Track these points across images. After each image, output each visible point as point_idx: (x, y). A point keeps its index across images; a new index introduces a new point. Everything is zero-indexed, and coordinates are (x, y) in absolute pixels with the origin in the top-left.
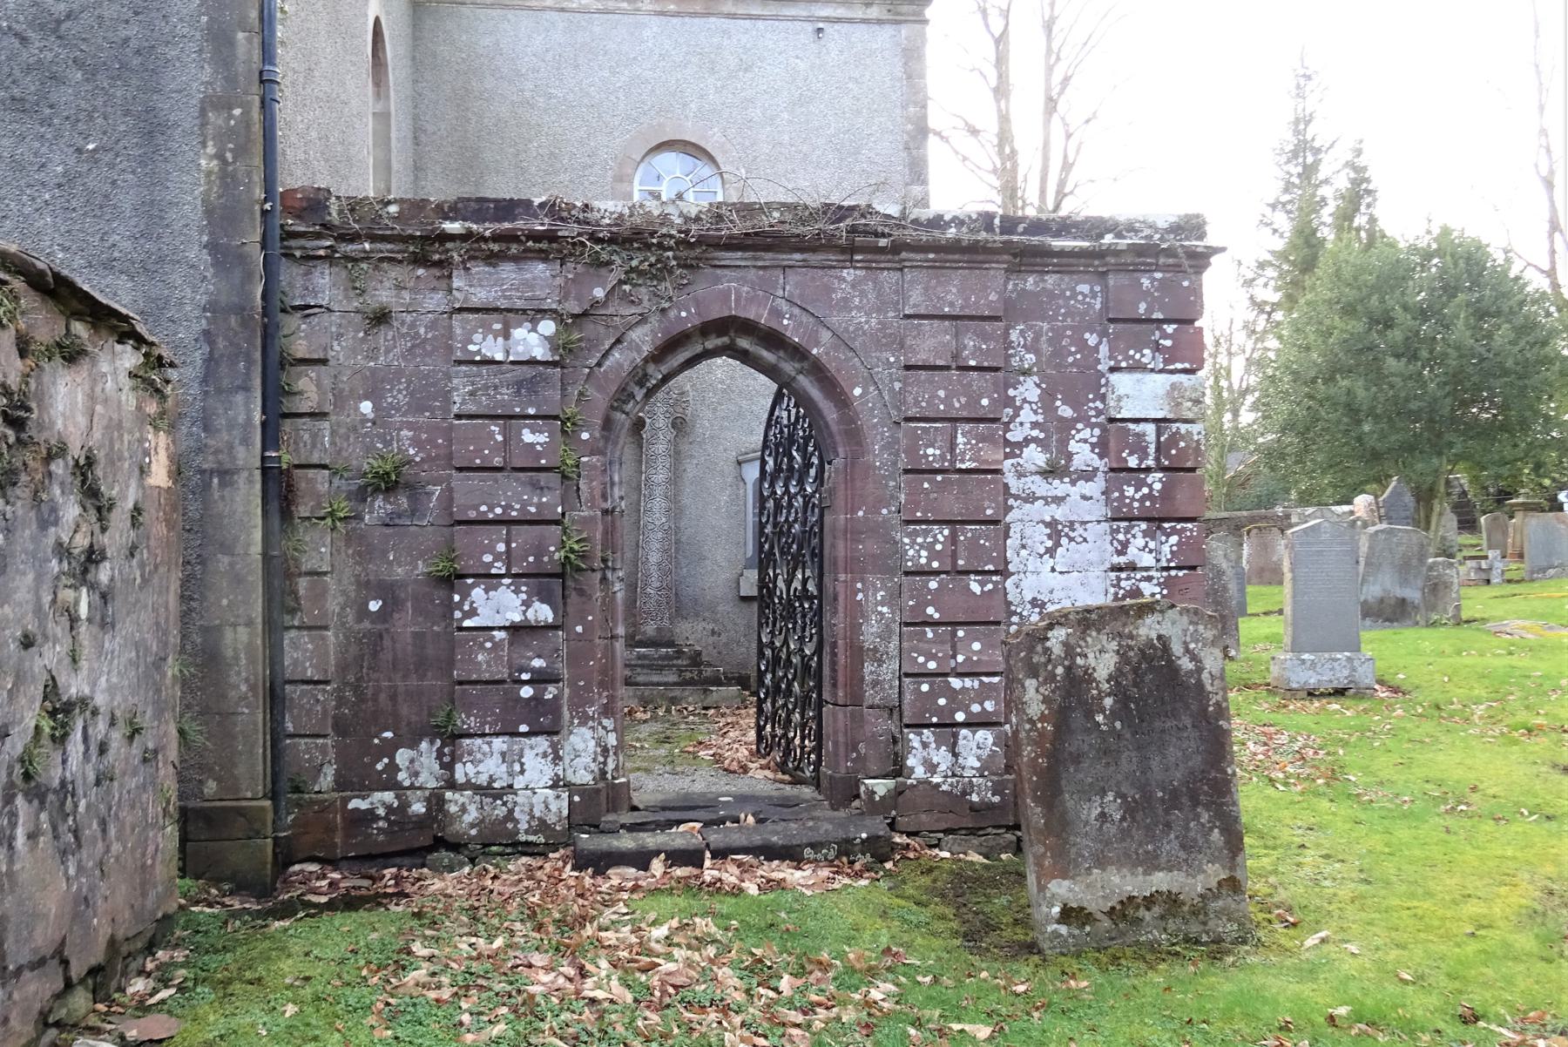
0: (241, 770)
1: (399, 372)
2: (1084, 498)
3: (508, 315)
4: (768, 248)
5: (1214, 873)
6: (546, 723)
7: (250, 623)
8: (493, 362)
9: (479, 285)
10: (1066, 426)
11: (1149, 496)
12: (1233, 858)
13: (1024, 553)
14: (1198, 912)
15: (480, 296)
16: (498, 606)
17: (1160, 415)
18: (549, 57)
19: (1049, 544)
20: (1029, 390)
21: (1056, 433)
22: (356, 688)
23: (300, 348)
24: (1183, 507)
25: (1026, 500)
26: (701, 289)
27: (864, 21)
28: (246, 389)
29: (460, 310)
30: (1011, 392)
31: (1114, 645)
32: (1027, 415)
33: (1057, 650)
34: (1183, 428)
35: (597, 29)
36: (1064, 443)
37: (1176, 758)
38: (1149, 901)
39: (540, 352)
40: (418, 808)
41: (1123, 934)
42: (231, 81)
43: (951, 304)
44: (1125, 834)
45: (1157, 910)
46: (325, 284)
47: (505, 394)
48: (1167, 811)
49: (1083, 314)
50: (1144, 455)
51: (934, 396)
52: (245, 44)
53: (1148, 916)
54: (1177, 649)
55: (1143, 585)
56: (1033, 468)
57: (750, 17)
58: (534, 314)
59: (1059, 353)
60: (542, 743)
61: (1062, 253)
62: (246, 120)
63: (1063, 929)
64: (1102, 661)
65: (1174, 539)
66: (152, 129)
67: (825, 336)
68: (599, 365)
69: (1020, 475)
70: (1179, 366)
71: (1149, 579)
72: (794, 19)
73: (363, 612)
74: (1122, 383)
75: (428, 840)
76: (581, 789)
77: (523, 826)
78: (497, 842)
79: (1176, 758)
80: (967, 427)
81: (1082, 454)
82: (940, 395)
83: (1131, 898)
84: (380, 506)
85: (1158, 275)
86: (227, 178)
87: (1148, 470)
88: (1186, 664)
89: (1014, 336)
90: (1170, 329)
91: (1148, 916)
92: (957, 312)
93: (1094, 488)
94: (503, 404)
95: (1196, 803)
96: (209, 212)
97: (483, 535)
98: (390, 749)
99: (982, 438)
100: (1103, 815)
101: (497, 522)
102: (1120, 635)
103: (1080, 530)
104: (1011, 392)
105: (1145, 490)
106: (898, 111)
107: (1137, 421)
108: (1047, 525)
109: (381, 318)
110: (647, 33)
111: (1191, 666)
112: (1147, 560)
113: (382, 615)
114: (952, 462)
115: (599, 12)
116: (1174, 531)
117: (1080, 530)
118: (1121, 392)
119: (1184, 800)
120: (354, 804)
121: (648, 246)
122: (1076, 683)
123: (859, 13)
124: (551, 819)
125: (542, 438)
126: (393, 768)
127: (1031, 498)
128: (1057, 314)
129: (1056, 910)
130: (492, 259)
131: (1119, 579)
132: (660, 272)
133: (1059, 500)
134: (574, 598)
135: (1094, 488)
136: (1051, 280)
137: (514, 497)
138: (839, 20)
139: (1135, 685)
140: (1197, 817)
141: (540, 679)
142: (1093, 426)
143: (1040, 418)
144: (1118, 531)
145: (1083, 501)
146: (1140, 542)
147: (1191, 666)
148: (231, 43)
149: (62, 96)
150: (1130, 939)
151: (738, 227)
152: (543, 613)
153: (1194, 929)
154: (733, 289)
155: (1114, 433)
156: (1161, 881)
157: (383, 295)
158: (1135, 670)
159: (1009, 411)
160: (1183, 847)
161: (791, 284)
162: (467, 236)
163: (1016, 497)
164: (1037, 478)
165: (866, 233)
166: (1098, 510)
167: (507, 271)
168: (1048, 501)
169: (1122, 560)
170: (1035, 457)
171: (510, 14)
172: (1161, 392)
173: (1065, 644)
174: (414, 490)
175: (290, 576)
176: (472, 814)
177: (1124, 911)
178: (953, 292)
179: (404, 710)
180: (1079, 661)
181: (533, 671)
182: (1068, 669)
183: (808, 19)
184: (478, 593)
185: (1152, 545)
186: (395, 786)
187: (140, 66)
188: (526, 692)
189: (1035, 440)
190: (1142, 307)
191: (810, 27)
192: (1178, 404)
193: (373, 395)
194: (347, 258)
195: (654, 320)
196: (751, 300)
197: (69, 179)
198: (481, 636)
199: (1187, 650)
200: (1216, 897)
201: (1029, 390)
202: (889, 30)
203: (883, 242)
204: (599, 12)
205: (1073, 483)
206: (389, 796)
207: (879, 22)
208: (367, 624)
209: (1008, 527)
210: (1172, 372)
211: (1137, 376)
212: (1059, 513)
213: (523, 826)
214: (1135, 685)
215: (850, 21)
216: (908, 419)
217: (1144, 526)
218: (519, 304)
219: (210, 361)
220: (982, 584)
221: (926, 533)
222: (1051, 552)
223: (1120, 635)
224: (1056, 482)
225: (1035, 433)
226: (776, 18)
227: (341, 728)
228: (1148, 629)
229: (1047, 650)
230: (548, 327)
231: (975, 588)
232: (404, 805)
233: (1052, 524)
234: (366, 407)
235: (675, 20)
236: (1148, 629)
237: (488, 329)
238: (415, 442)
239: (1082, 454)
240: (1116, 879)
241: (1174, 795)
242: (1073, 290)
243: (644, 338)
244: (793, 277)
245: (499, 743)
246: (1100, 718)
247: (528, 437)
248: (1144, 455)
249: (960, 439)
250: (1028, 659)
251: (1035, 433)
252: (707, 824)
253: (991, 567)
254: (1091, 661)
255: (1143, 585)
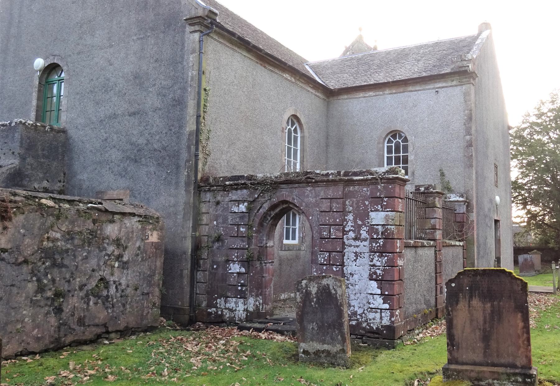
0: (185, 300)
1: (221, 215)
2: (364, 246)
3: (239, 202)
4: (290, 183)
5: (339, 347)
6: (243, 296)
7: (187, 269)
8: (235, 212)
9: (235, 195)
10: (360, 227)
11: (379, 246)
12: (344, 344)
13: (348, 260)
14: (334, 356)
15: (234, 198)
16: (235, 268)
17: (383, 223)
18: (361, 111)
19: (355, 258)
20: (350, 217)
21: (357, 229)
22: (211, 285)
23: (204, 210)
24: (389, 248)
25: (349, 246)
26: (278, 194)
27: (451, 86)
28: (189, 220)
29: (231, 201)
30: (346, 218)
31: (316, 286)
32: (350, 224)
33: (304, 286)
34: (389, 227)
35: (374, 101)
36: (359, 231)
37: (330, 316)
38: (323, 352)
39: (244, 210)
40: (220, 313)
41: (316, 359)
42: (190, 156)
43: (330, 195)
44: (318, 334)
45: (325, 354)
46: (208, 196)
47: (238, 220)
48: (328, 329)
49: (365, 196)
50: (378, 235)
51: (326, 219)
52: (193, 148)
53: (323, 356)
54: (331, 288)
55: (377, 271)
56: (351, 238)
57: (416, 91)
58: (244, 202)
59: (358, 207)
60: (242, 300)
61: (357, 180)
62: (192, 164)
63: (303, 356)
64: (314, 289)
65: (386, 258)
66: (178, 167)
67: (304, 204)
68: (258, 212)
69: (348, 240)
70: (388, 210)
71: (379, 269)
72: (429, 89)
73: (213, 268)
74: (372, 215)
75: (219, 321)
76: (250, 312)
77: (237, 319)
78: (232, 322)
79: (330, 316)
80: (333, 227)
81: (364, 234)
82: (327, 219)
83: (319, 350)
84: (217, 245)
85: (383, 185)
86: (188, 176)
87: (380, 239)
88: (333, 292)
89: (347, 203)
90: (386, 199)
91: (323, 356)
92: (331, 197)
93: (366, 243)
94: (237, 222)
95: (334, 328)
96: (185, 184)
97: (233, 252)
98: (216, 299)
99: (337, 230)
100: (313, 328)
101: (235, 249)
102: (318, 283)
103: (363, 255)
104: (346, 218)
105: (378, 244)
106: (462, 113)
107: (377, 225)
108: (354, 253)
109: (218, 203)
110: (387, 100)
111: (334, 292)
112: (378, 264)
113: (216, 269)
114: (330, 236)
115: (374, 96)
116: (386, 256)
117: (363, 255)
118: (372, 217)
119: (332, 327)
120: (209, 310)
121: (265, 185)
122: (308, 294)
123: (450, 84)
124: (242, 318)
125: (244, 230)
126: (217, 303)
127: (350, 246)
128: (358, 196)
129: (302, 350)
130: (236, 189)
131: (371, 269)
132: (267, 191)
133: (357, 246)
134: (251, 267)
135: (366, 243)
136: (356, 187)
137: (239, 243)
138: (443, 87)
139: (321, 296)
140: (335, 332)
141: (242, 285)
142: (367, 226)
143: (353, 224)
144: (371, 255)
145: (364, 247)
146: (377, 259)
147: (334, 292)
148: (191, 148)
149: (165, 162)
150: (318, 361)
151: (283, 179)
152: (243, 270)
153: (333, 361)
154: (285, 193)
155: (372, 229)
156: (326, 347)
157: (219, 198)
158: (321, 292)
159: (345, 222)
160: (331, 339)
161: (296, 192)
162: (231, 185)
163: (347, 245)
164: (352, 240)
165: (311, 179)
166: (367, 250)
167: (239, 192)
168: (355, 246)
169: (372, 263)
170: (352, 235)
171: (351, 100)
172: (383, 217)
173: (306, 284)
174: (223, 241)
175: (198, 260)
176: (228, 316)
177: (317, 353)
178: (331, 192)
179: (219, 290)
180: (309, 289)
181: (241, 284)
182: (306, 291)
183: (433, 89)
184: (231, 265)
185: (380, 259)
186: (217, 307)
187: (176, 155)
188: (239, 288)
189: (352, 230)
190: (378, 194)
191: (434, 91)
192: (388, 220)
193: (216, 220)
194: (213, 190)
195: (268, 201)
196: (288, 196)
197: (165, 178)
198: (232, 275)
199: (333, 288)
200: (339, 353)
201: (350, 217)
202: (459, 88)
203: (314, 181)
204: (374, 96)
205: (361, 242)
206: (215, 309)
207: (456, 86)
208: (213, 271)
209: (345, 253)
210: (387, 211)
211: (377, 213)
212: (358, 250)
213: (237, 319)
214: (321, 296)
215: (446, 87)
216: (321, 225)
217: (378, 254)
218: (241, 199)
219: (184, 214)
220: (336, 268)
221: (323, 254)
222: (355, 260)
223: (318, 283)
224: (357, 242)
225: (352, 228)
226: (424, 90)
227: (208, 293)
228: (325, 282)
229: (302, 286)
230: (246, 204)
231: (334, 269)
232: (217, 312)
233: (356, 253)
234: (215, 223)
235: (395, 95)
236: (325, 282)
237: (235, 204)
238: (223, 230)
239: (364, 234)
240: (315, 345)
241: (330, 325)
242: (362, 190)
243: (266, 206)
244: (297, 190)
245: (234, 299)
246: (313, 304)
247: (242, 229)
248: (378, 235)
249: (332, 230)
250: (297, 287)
251: (352, 228)
252: (274, 324)
253: (338, 264)
254: (311, 289)
255: (377, 271)
